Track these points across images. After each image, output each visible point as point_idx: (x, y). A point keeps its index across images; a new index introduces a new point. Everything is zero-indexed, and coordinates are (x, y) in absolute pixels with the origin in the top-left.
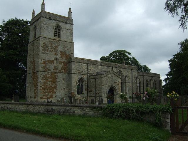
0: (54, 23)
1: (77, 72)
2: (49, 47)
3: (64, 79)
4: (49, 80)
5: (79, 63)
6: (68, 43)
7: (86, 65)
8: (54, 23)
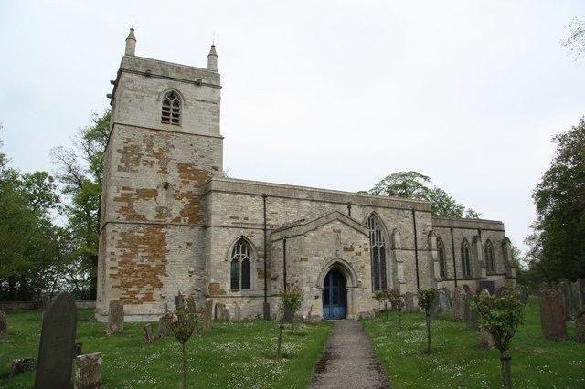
2: (144, 152)
3: (189, 244)
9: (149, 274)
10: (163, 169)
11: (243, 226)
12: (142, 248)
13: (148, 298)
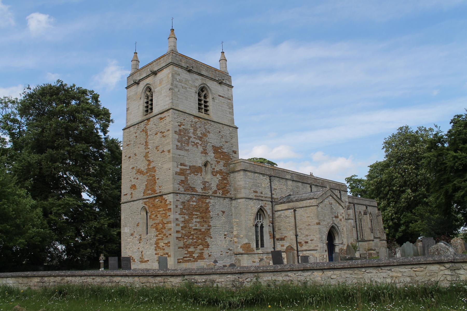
0: (199, 81)
1: (252, 195)
2: (191, 135)
3: (223, 212)
4: (194, 215)
5: (255, 173)
6: (225, 127)
7: (268, 178)
8: (197, 79)
9: (200, 237)
10: (205, 150)
11: (261, 198)
12: (196, 215)
13: (201, 257)
